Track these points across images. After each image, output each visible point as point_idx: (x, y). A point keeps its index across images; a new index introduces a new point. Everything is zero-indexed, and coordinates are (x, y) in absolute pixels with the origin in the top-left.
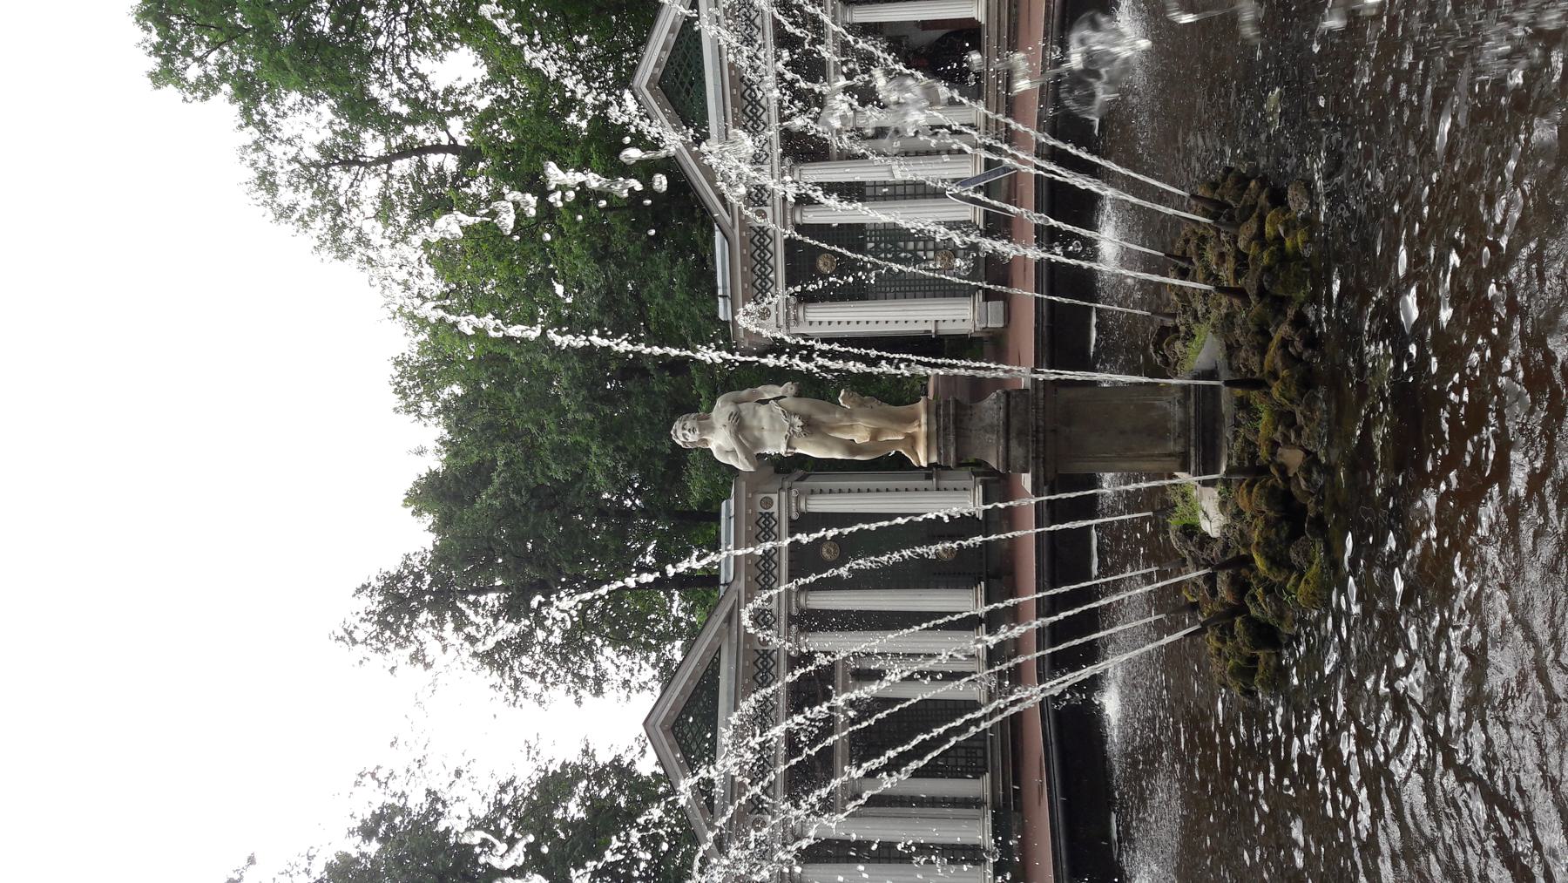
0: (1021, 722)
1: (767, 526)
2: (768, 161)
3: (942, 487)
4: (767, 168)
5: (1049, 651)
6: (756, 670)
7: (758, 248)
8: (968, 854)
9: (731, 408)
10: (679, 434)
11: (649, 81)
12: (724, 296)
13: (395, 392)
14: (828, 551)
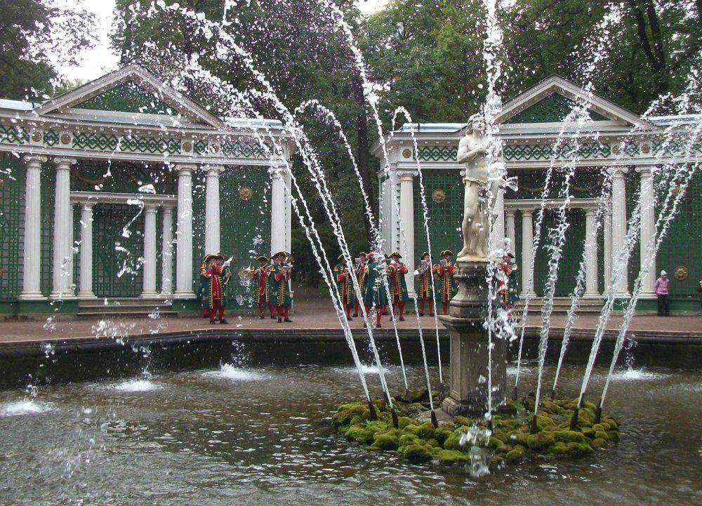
1: (544, 152)
5: (397, 337)
10: (477, 119)
12: (419, 128)
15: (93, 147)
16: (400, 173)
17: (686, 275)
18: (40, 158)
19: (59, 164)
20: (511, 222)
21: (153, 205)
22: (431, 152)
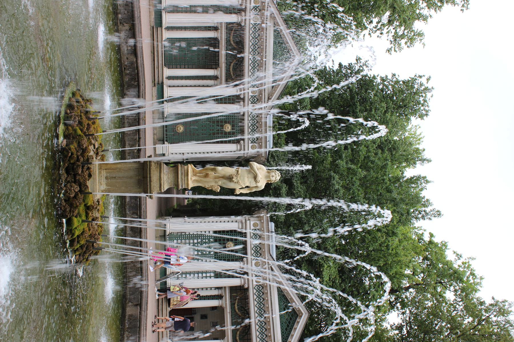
0: (138, 49)
1: (254, 52)
2: (254, 286)
3: (182, 154)
4: (255, 283)
6: (258, 38)
7: (258, 252)
8: (176, 10)
9: (259, 184)
10: (277, 175)
11: (301, 316)
13: (420, 175)
14: (228, 128)
15: (251, 65)
16: (244, 221)
17: (178, 132)
18: (244, 4)
19: (241, 15)
20: (215, 293)
21: (219, 73)
22: (261, 296)
